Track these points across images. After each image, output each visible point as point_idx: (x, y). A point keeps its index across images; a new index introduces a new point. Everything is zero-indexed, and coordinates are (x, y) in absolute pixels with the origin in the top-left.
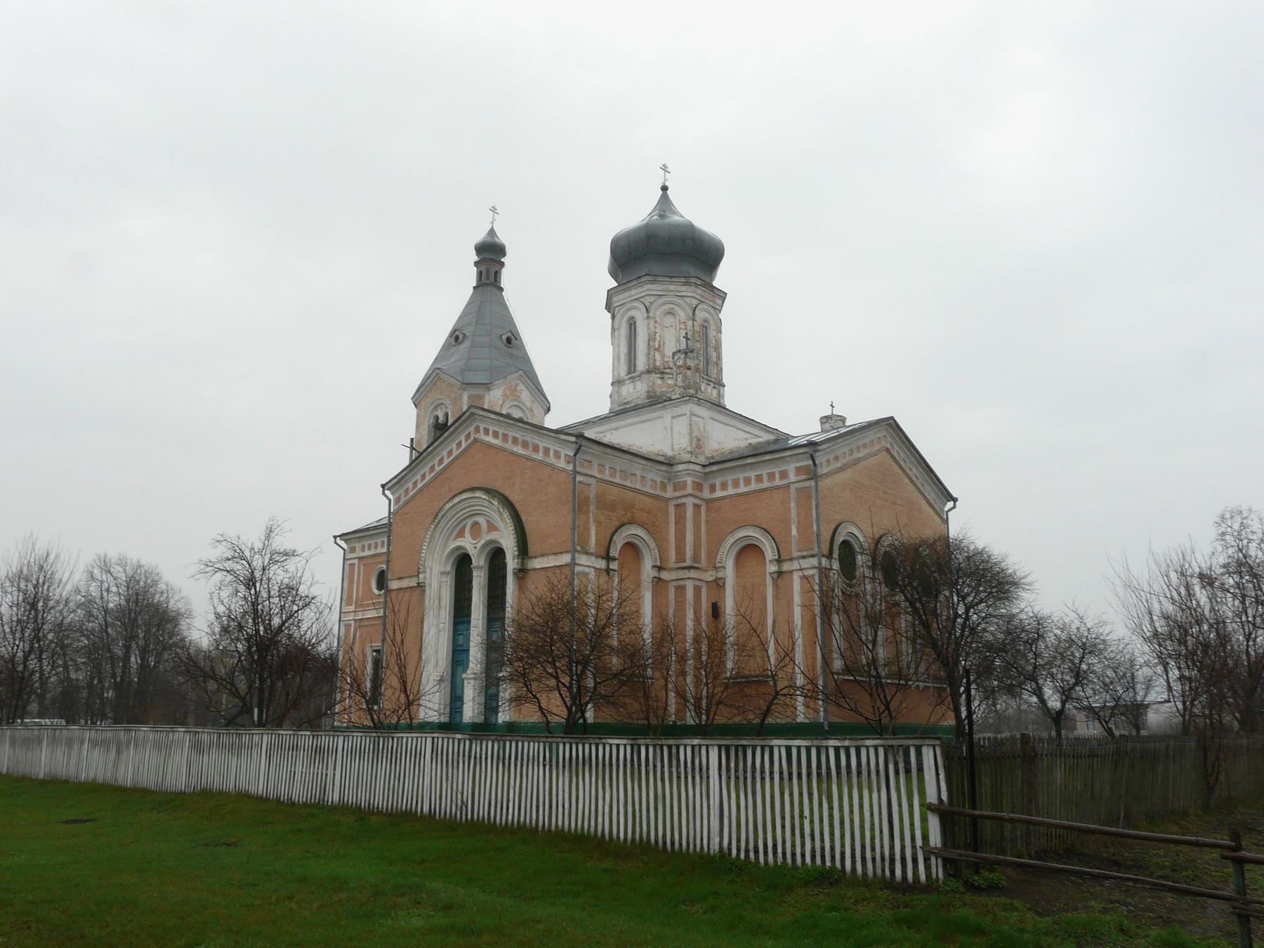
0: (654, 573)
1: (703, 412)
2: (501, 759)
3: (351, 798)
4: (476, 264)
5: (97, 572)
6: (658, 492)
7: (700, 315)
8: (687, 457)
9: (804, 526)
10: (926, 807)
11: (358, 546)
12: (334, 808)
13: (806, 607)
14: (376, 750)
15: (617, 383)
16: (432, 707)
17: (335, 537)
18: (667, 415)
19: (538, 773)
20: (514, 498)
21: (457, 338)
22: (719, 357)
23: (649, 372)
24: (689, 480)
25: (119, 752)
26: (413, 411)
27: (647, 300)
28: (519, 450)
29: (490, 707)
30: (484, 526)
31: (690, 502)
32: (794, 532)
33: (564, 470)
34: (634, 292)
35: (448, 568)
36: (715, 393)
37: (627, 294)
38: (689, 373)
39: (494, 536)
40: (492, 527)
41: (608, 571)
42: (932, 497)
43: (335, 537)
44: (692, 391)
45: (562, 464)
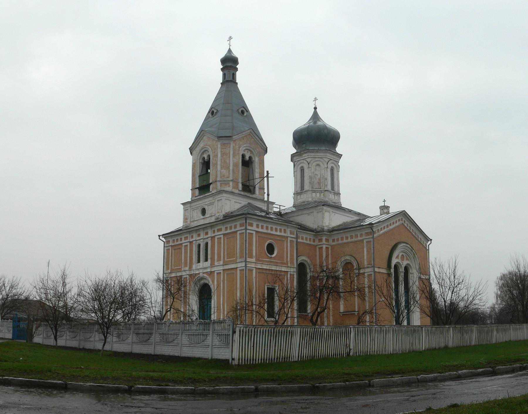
4: (222, 69)
6: (312, 243)
11: (171, 240)
15: (296, 194)
17: (159, 236)
21: (213, 113)
27: (309, 160)
31: (324, 247)
43: (159, 236)
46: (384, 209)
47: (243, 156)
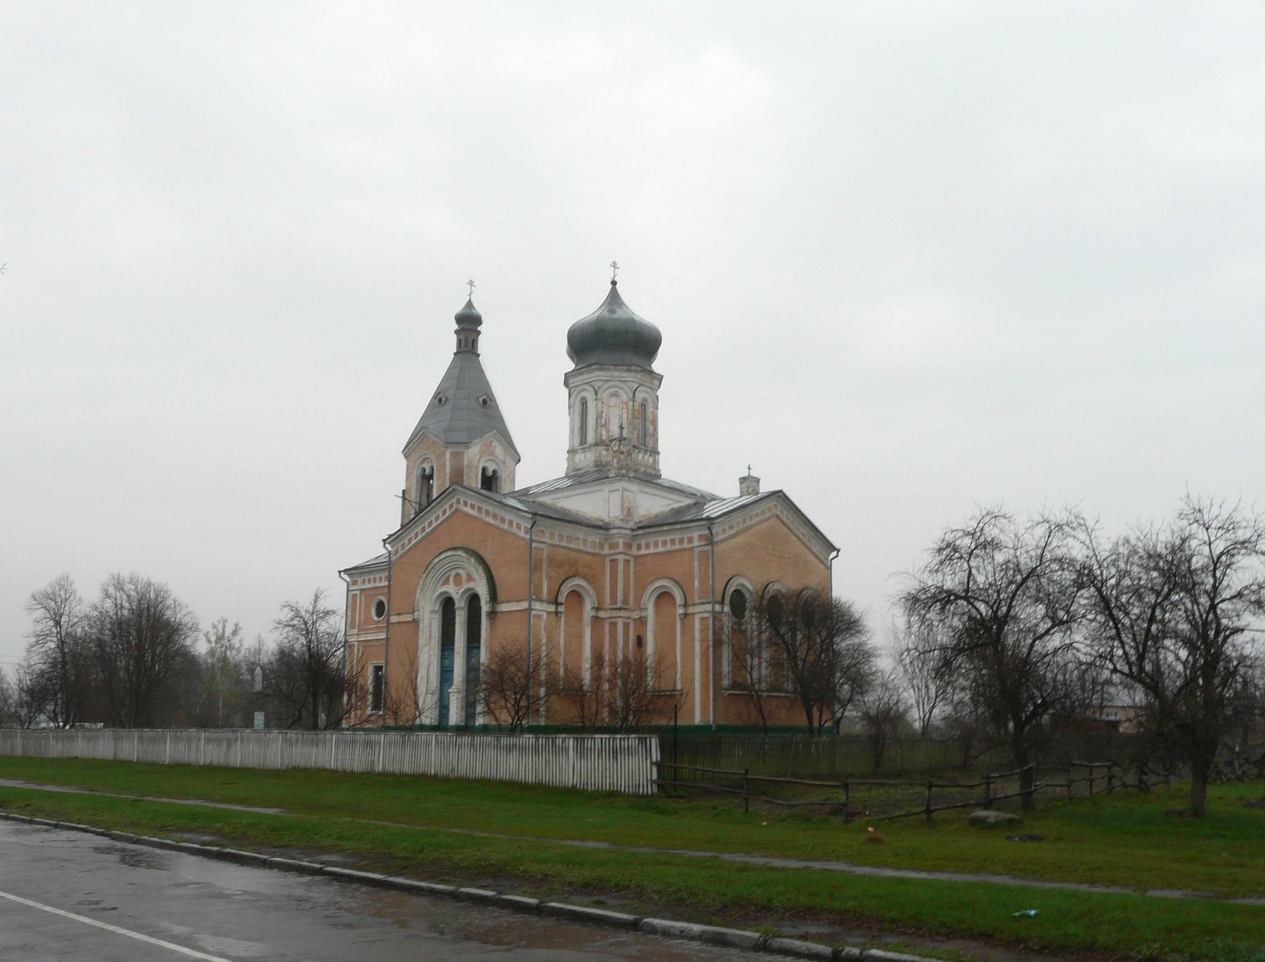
0: (593, 613)
1: (633, 487)
2: (472, 745)
3: (389, 768)
5: (111, 590)
6: (597, 551)
7: (640, 396)
8: (619, 523)
9: (703, 581)
10: (652, 763)
11: (360, 580)
12: (379, 774)
13: (703, 640)
14: (404, 742)
15: (572, 452)
16: (428, 718)
18: (606, 488)
19: (491, 753)
20: (488, 557)
21: (440, 400)
22: (655, 429)
23: (596, 445)
24: (621, 541)
25: (229, 746)
26: (404, 462)
27: (596, 385)
28: (490, 520)
29: (469, 706)
30: (464, 577)
31: (621, 558)
32: (696, 584)
33: (523, 539)
34: (585, 376)
35: (437, 608)
36: (651, 460)
37: (581, 378)
38: (622, 457)
39: (471, 585)
40: (470, 578)
41: (557, 613)
42: (817, 548)
44: (624, 472)
45: (522, 533)
46: (749, 482)
47: (484, 470)
